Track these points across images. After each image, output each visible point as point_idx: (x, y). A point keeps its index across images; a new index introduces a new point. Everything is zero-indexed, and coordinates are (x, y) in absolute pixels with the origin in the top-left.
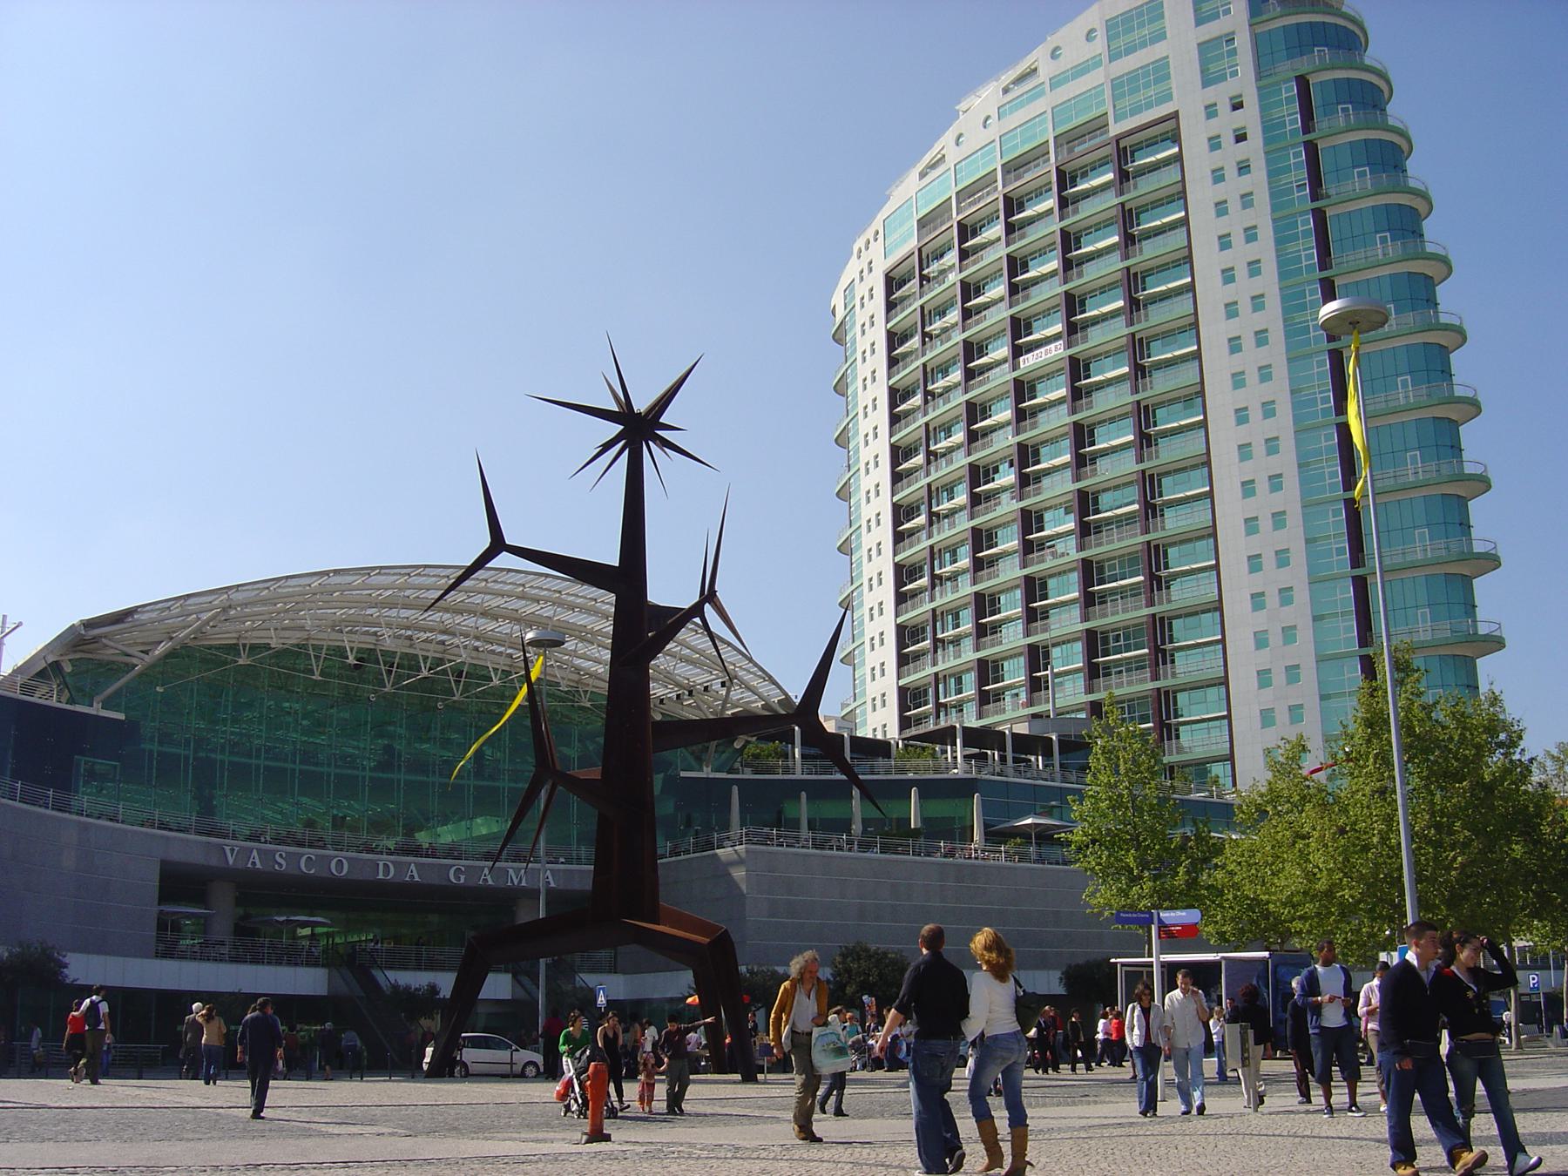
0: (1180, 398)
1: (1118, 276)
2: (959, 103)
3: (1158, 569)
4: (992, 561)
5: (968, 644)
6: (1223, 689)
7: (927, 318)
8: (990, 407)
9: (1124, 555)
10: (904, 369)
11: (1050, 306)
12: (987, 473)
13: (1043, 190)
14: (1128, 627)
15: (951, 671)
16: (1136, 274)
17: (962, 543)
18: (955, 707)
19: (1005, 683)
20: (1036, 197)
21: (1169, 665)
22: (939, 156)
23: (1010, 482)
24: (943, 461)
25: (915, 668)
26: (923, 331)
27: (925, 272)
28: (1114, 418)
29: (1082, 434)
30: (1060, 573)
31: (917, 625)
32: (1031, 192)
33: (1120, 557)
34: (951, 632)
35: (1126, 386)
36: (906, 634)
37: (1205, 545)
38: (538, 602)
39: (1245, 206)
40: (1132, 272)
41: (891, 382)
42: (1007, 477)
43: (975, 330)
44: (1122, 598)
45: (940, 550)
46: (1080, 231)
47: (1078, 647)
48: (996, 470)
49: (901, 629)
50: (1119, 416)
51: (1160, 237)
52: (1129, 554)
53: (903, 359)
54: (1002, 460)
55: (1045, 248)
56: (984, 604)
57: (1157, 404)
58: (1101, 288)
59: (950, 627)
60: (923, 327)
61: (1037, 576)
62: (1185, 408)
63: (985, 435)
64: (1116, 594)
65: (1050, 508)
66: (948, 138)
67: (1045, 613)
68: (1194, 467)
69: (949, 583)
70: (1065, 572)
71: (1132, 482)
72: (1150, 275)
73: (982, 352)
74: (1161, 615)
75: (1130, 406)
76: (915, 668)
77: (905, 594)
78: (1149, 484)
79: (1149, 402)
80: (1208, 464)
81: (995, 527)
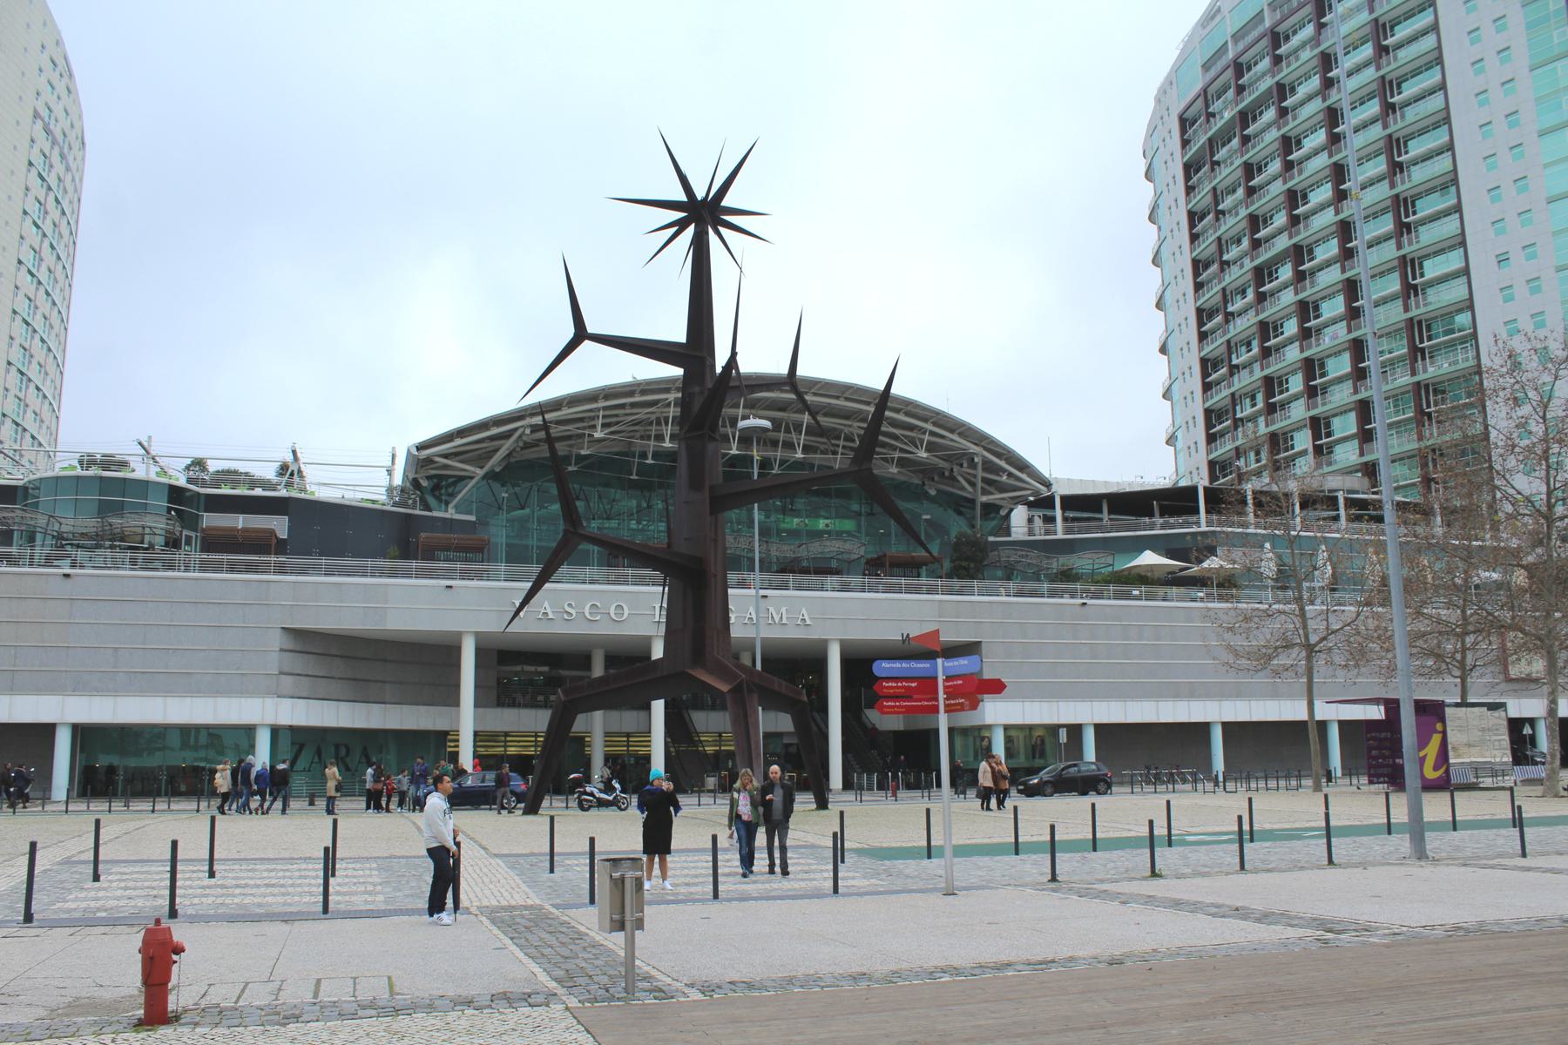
0: (1435, 187)
1: (1374, 86)
3: (1414, 278)
4: (1284, 405)
5: (1257, 366)
6: (1464, 279)
7: (1225, 247)
8: (1287, 380)
9: (1397, 395)
10: (1208, 292)
11: (1316, 122)
13: (1306, 21)
15: (1244, 391)
21: (1420, 296)
22: (1216, 8)
26: (1211, 161)
27: (1220, 208)
28: (1377, 212)
30: (1341, 413)
32: (1301, 77)
33: (1394, 396)
37: (1447, 156)
39: (1511, 126)
40: (1387, 80)
41: (1199, 303)
42: (1286, 272)
43: (1274, 368)
44: (1397, 432)
47: (1352, 416)
49: (1208, 413)
51: (1428, 163)
56: (1271, 385)
57: (1415, 195)
58: (1367, 156)
59: (1253, 462)
60: (1221, 256)
61: (1315, 357)
62: (1442, 196)
63: (1272, 295)
65: (1325, 297)
67: (1330, 448)
68: (1452, 248)
69: (1250, 424)
70: (1345, 412)
71: (1395, 267)
72: (1405, 81)
73: (1272, 276)
74: (1419, 318)
75: (1396, 261)
78: (1408, 266)
79: (1400, 134)
80: (1463, 244)
81: (1291, 431)
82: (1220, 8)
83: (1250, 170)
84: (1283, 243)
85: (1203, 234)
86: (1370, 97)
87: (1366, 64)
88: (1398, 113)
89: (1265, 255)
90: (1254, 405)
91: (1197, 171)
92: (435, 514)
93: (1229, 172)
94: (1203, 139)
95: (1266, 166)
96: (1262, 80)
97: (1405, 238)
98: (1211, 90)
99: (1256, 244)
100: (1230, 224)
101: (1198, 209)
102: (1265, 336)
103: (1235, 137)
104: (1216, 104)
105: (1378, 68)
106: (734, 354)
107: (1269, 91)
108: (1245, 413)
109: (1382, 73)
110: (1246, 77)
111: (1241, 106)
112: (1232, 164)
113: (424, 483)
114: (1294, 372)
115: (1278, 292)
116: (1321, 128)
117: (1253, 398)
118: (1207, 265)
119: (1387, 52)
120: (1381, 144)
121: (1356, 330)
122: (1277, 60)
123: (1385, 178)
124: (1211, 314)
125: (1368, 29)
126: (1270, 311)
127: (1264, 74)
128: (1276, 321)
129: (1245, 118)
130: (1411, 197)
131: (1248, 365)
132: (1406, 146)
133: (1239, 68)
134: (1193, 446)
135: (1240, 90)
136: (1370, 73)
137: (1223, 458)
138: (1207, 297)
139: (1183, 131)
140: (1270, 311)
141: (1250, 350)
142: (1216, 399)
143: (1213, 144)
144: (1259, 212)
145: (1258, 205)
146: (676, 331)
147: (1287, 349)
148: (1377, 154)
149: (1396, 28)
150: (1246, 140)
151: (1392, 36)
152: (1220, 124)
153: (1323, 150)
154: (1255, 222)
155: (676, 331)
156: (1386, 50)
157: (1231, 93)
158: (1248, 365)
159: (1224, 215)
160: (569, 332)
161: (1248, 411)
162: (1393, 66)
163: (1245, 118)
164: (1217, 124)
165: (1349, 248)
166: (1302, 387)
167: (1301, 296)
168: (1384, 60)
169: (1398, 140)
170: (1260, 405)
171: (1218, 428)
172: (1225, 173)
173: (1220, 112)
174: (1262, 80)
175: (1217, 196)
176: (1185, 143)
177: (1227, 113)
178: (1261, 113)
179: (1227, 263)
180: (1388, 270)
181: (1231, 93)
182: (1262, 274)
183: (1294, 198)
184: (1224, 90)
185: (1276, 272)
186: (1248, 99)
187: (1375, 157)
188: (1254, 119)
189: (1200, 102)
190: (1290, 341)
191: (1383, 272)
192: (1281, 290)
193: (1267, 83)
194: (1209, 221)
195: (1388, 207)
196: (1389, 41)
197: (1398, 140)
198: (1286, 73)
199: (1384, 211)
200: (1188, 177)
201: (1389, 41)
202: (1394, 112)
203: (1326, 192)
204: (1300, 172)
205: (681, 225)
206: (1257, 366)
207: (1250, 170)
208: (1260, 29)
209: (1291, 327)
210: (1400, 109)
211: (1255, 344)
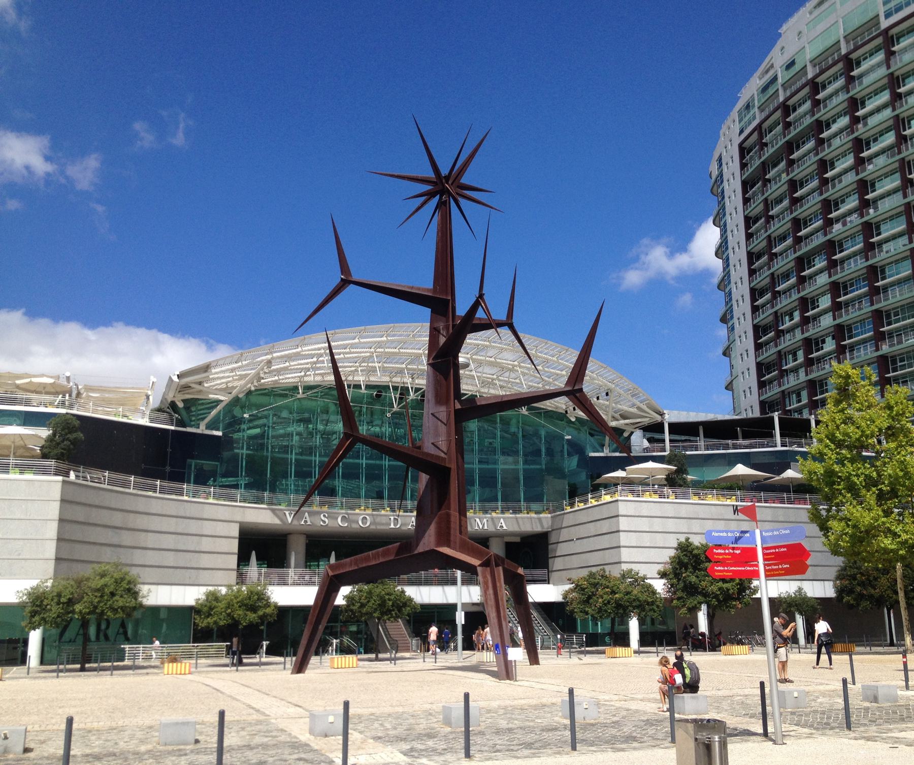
1: (891, 122)
2: (781, 26)
5: (802, 372)
8: (817, 300)
9: (904, 305)
12: (817, 344)
14: (909, 352)
15: (784, 310)
16: (898, 77)
17: (799, 348)
18: (797, 412)
19: (816, 267)
20: (834, 80)
22: (770, 65)
23: (815, 186)
24: (788, 336)
25: (770, 389)
28: (893, 216)
29: (859, 145)
31: (774, 401)
34: (795, 405)
35: (900, 194)
36: (762, 368)
38: (524, 729)
43: (812, 331)
45: (782, 314)
46: (864, 97)
48: (823, 342)
50: (896, 214)
52: (907, 304)
53: (762, 307)
54: (827, 335)
55: (854, 234)
61: (845, 324)
64: (901, 331)
66: (776, 50)
75: (903, 207)
76: (770, 389)
77: (764, 382)
79: (905, 115)
82: (773, 64)
83: (794, 185)
84: (819, 240)
85: (756, 233)
86: (888, 130)
87: (884, 106)
88: (909, 142)
89: (804, 249)
90: (795, 360)
91: (752, 187)
92: (189, 430)
93: (776, 189)
94: (757, 163)
95: (810, 221)
96: (803, 117)
97: (903, 147)
98: (766, 125)
99: (798, 240)
100: (777, 228)
101: (752, 214)
102: (809, 351)
103: (783, 160)
104: (768, 136)
105: (894, 110)
106: (481, 296)
107: (810, 126)
108: (788, 366)
109: (896, 113)
110: (792, 117)
111: (787, 138)
112: (783, 219)
113: (181, 405)
114: (823, 294)
115: (811, 235)
116: (849, 153)
117: (799, 395)
118: (756, 220)
119: (901, 98)
120: (902, 208)
121: (862, 172)
122: (816, 103)
123: (904, 234)
124: (762, 293)
125: (886, 81)
126: (808, 290)
127: (805, 114)
128: (814, 297)
129: (791, 147)
130: (907, 117)
131: (791, 330)
132: (909, 123)
133: (786, 109)
134: (745, 353)
135: (788, 125)
136: (888, 113)
137: (771, 399)
138: (759, 279)
139: (742, 156)
140: (808, 290)
141: (793, 319)
142: (765, 355)
143: (765, 167)
144: (801, 217)
145: (801, 212)
146: (424, 282)
147: (822, 318)
148: (892, 173)
149: (901, 40)
150: (791, 163)
151: (904, 86)
152: (771, 151)
153: (850, 170)
154: (797, 224)
155: (424, 282)
156: (900, 96)
157: (779, 128)
158: (791, 330)
159: (773, 219)
160: (338, 277)
161: (791, 365)
162: (905, 107)
163: (791, 147)
164: (769, 151)
165: (867, 199)
166: (835, 346)
167: (834, 278)
168: (897, 104)
169: (903, 119)
170: (805, 400)
171: (764, 339)
172: (774, 188)
173: (771, 142)
174: (803, 117)
175: (768, 205)
176: (743, 166)
177: (776, 140)
178: (803, 143)
179: (772, 217)
180: (902, 259)
181: (779, 128)
182: (802, 262)
183: (828, 206)
184: (776, 124)
185: (814, 261)
186: (793, 132)
187: (891, 175)
188: (798, 148)
189: (756, 135)
190: (825, 312)
191: (898, 260)
192: (817, 274)
193: (808, 120)
194: (762, 224)
195: (902, 212)
196: (902, 90)
197: (903, 119)
198: (823, 114)
199: (898, 215)
200: (745, 191)
201: (902, 90)
202: (906, 141)
203: (854, 201)
204: (825, 107)
205: (430, 195)
206: (802, 372)
207: (794, 185)
208: (804, 80)
209: (825, 302)
210: (905, 96)
211: (797, 315)
